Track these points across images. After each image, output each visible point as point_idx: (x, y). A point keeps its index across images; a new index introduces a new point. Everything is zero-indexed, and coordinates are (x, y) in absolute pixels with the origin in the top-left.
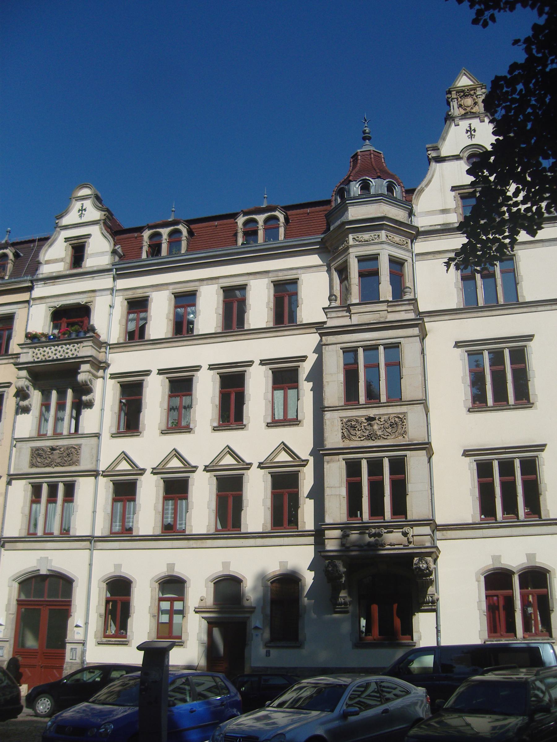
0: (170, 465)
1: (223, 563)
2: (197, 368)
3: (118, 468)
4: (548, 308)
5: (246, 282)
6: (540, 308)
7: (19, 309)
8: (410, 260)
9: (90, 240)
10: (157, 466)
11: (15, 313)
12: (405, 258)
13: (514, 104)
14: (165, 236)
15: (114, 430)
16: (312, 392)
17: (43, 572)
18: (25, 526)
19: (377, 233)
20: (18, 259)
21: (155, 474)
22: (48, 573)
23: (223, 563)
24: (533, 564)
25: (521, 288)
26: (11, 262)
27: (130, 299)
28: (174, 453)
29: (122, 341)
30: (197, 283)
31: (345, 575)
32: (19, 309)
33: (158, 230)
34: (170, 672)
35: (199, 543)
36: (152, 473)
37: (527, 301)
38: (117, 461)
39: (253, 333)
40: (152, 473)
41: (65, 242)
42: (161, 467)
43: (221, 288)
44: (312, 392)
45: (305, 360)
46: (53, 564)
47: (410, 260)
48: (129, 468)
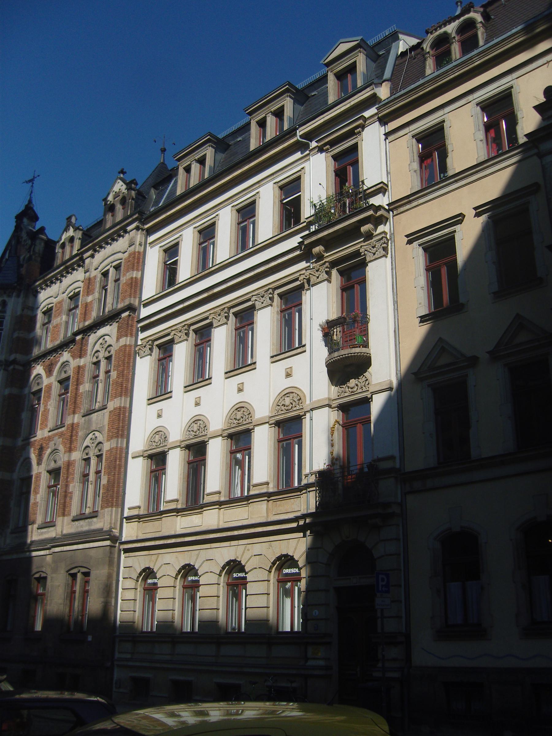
7: (517, 78)
11: (512, 87)
16: (425, 328)
20: (490, 22)
26: (481, 25)
32: (517, 78)
44: (425, 328)
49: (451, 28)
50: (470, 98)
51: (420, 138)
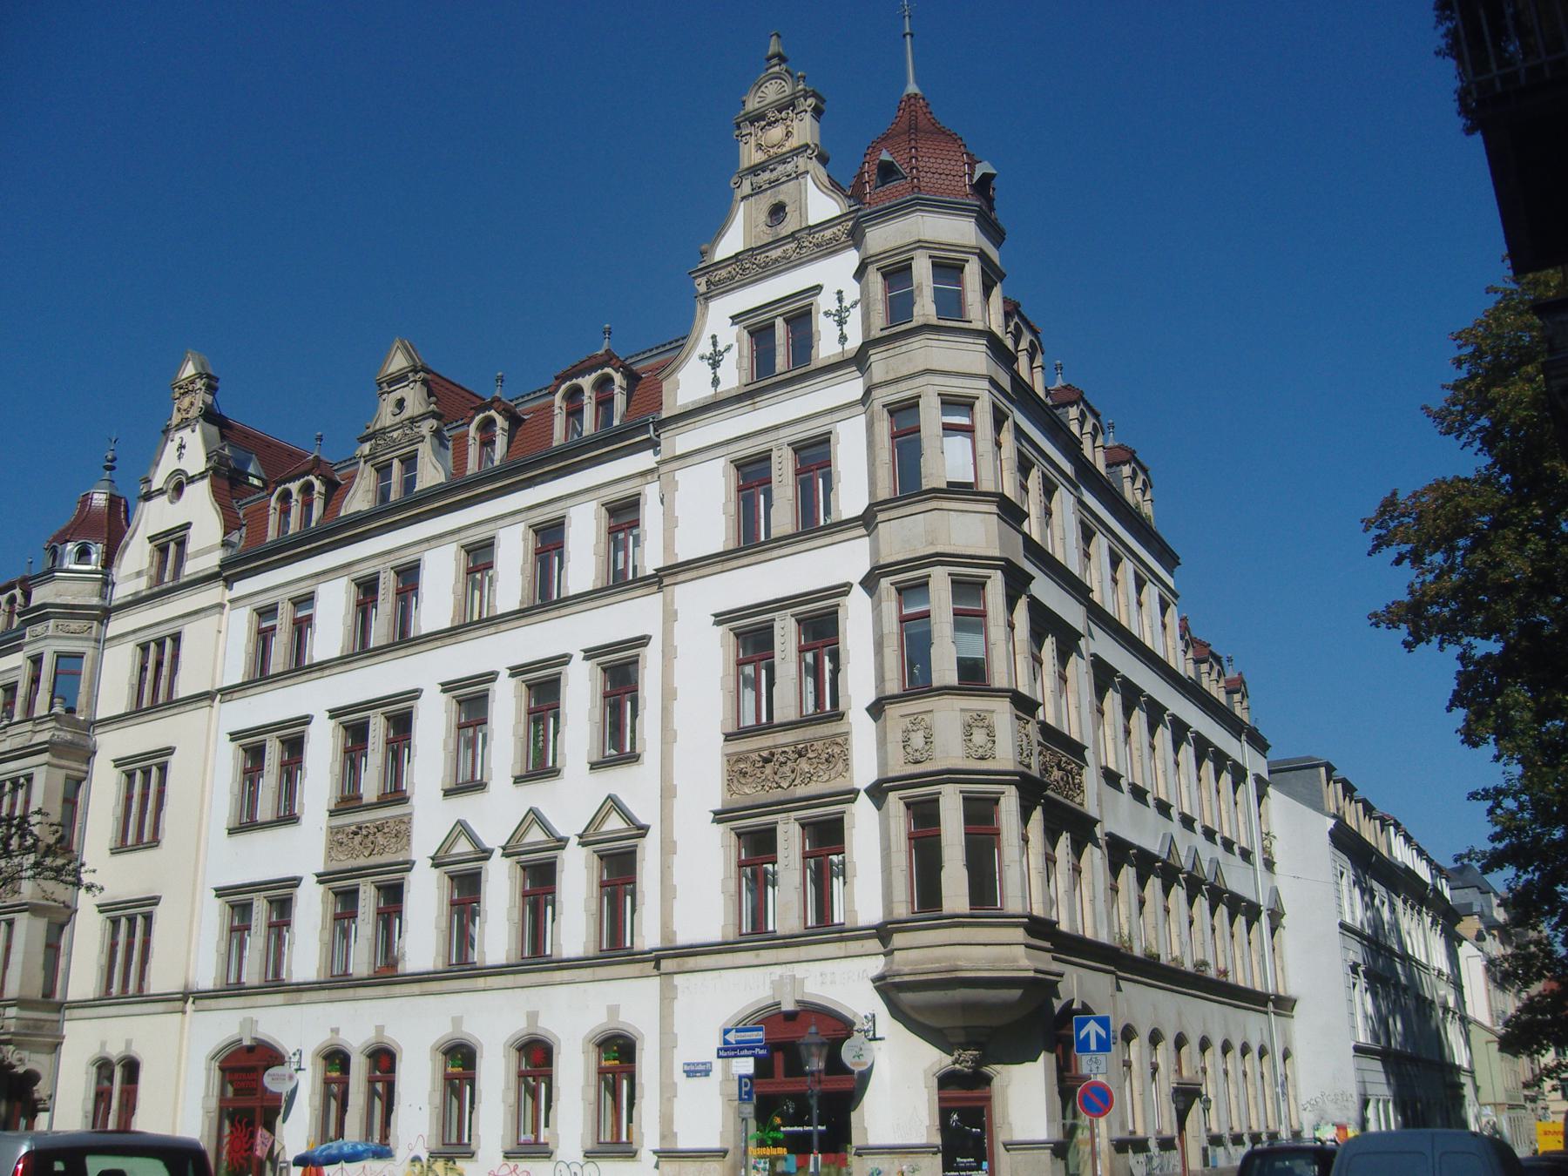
0: (455, 851)
1: (376, 1027)
2: (564, 660)
3: (455, 851)
4: (719, 567)
5: (638, 489)
6: (503, 627)
8: (90, 652)
9: (192, 532)
10: (585, 831)
12: (82, 650)
13: (905, 83)
14: (588, 391)
15: (793, 713)
17: (788, 1006)
18: (732, 919)
19: (44, 624)
21: (584, 844)
22: (798, 1009)
23: (376, 1027)
24: (458, 1036)
25: (837, 495)
27: (739, 459)
28: (532, 816)
29: (731, 547)
30: (638, 481)
31: (1499, 933)
33: (574, 381)
34: (1393, 1127)
35: (416, 988)
36: (503, 855)
37: (844, 518)
38: (450, 840)
39: (429, 641)
40: (503, 855)
41: (734, 324)
42: (513, 843)
43: (731, 462)
45: (648, 644)
46: (260, 1029)
47: (90, 652)
48: (544, 837)
49: (586, 382)
50: (456, 537)
51: (741, 465)
